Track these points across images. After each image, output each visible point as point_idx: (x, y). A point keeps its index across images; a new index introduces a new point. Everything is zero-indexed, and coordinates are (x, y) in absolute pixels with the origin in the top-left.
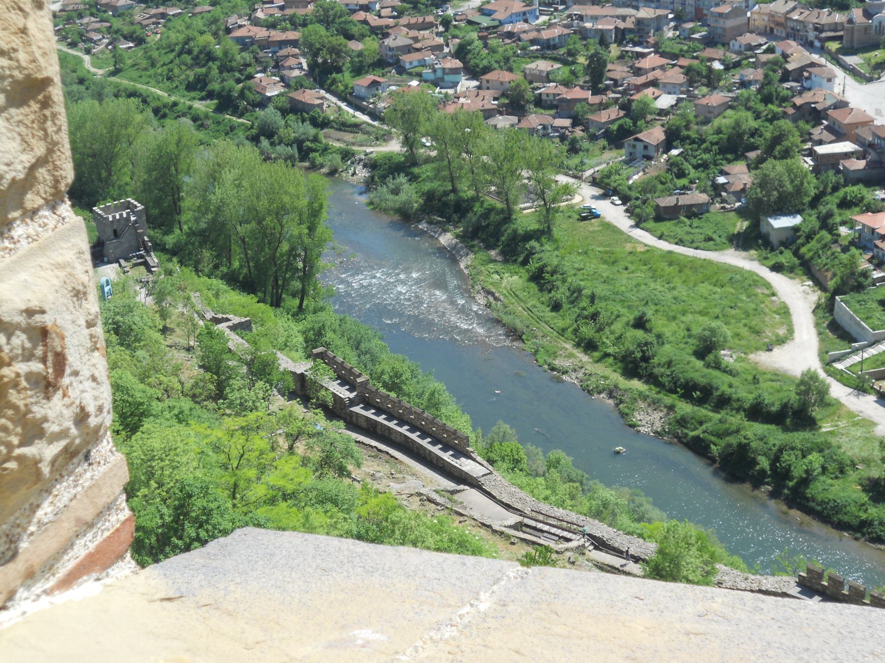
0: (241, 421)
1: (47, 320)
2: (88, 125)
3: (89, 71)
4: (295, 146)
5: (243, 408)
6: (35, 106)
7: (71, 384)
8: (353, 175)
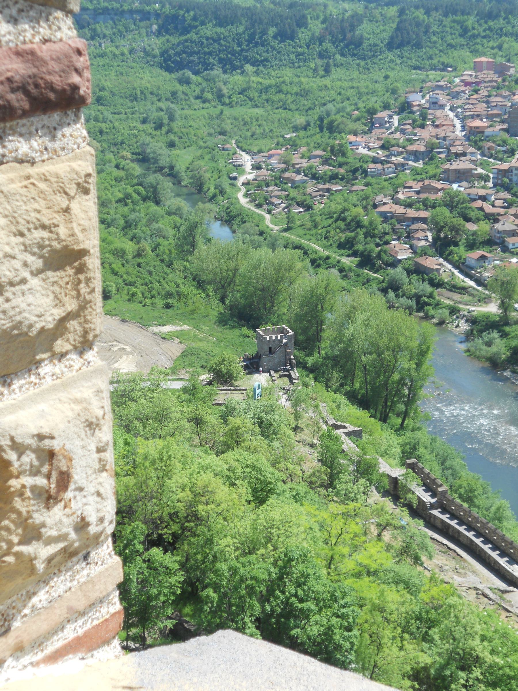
0: (342, 508)
1: (56, 445)
3: (268, 227)
4: (414, 299)
5: (347, 498)
6: (70, 271)
7: (75, 497)
8: (456, 327)
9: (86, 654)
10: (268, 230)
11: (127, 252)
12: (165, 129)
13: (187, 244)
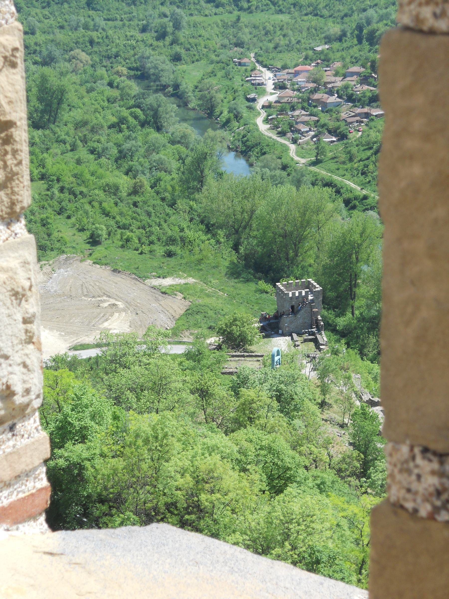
2: (283, 208)
3: (292, 159)
9: (11, 526)
10: (292, 164)
11: (121, 188)
12: (168, 39)
13: (194, 180)
